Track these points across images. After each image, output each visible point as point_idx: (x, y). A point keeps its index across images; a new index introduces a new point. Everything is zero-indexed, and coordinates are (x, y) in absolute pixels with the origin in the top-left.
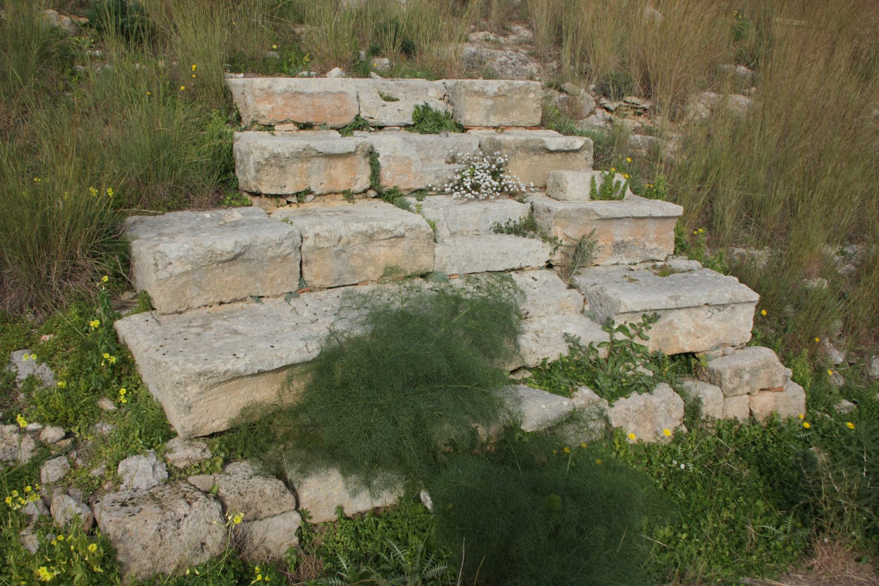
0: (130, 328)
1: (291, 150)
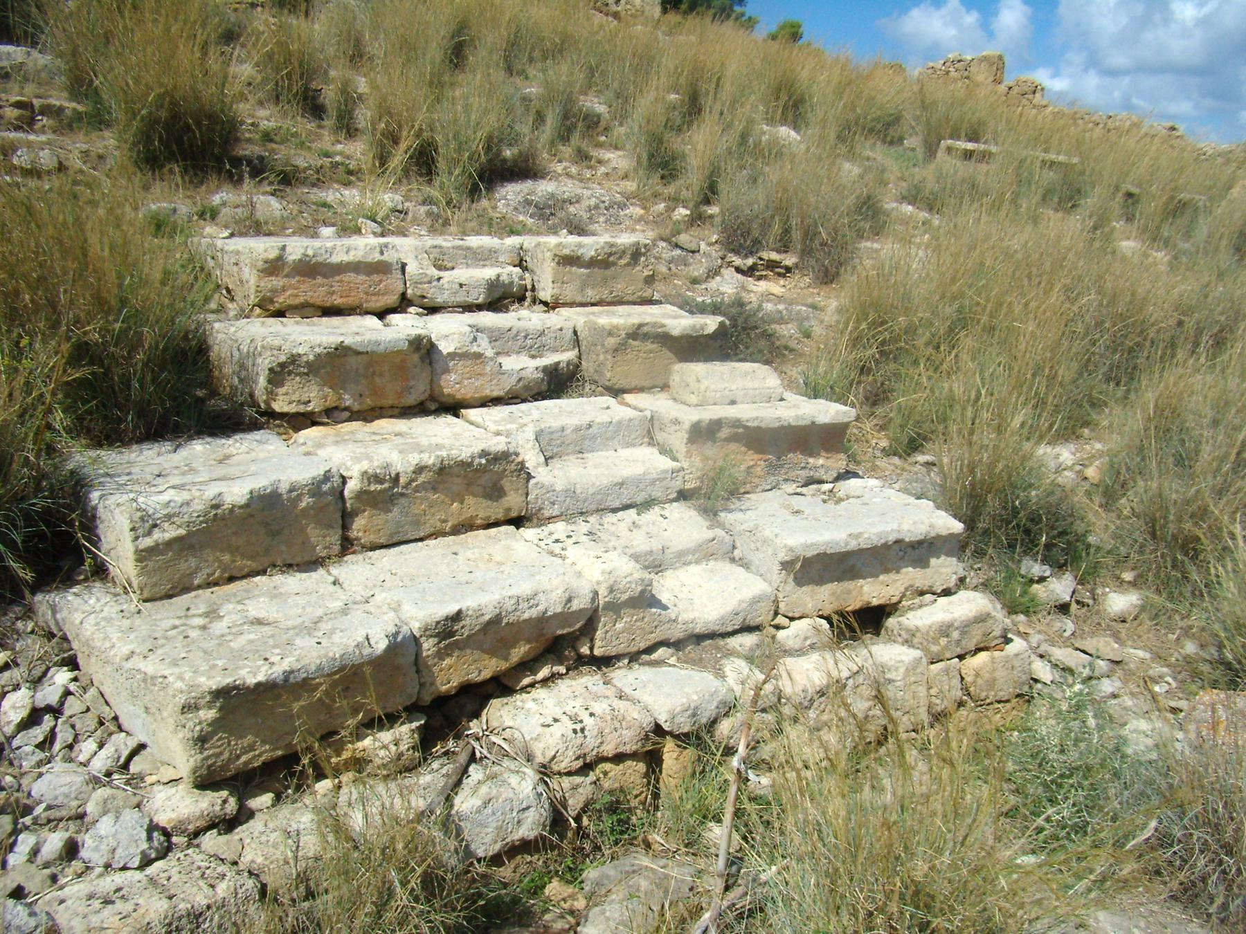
0: (97, 624)
1: (317, 350)
